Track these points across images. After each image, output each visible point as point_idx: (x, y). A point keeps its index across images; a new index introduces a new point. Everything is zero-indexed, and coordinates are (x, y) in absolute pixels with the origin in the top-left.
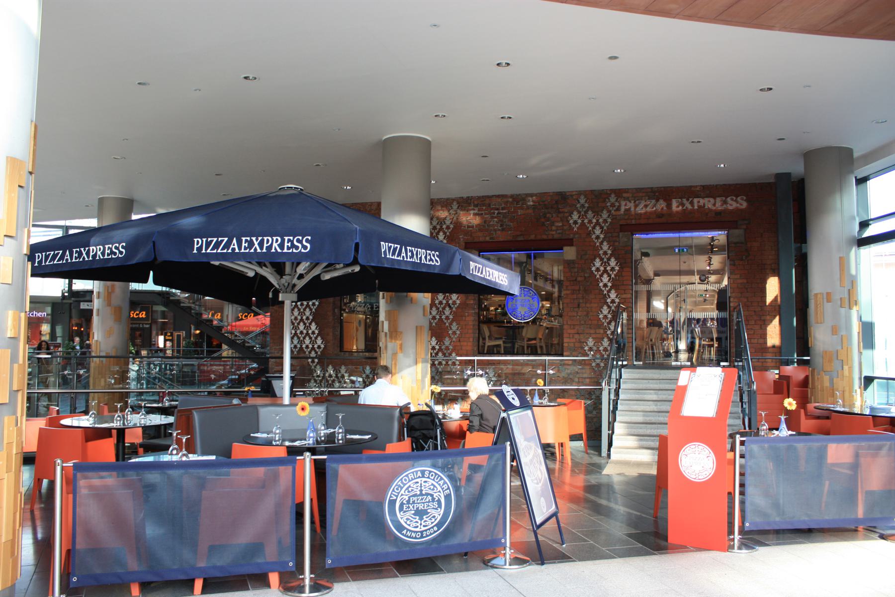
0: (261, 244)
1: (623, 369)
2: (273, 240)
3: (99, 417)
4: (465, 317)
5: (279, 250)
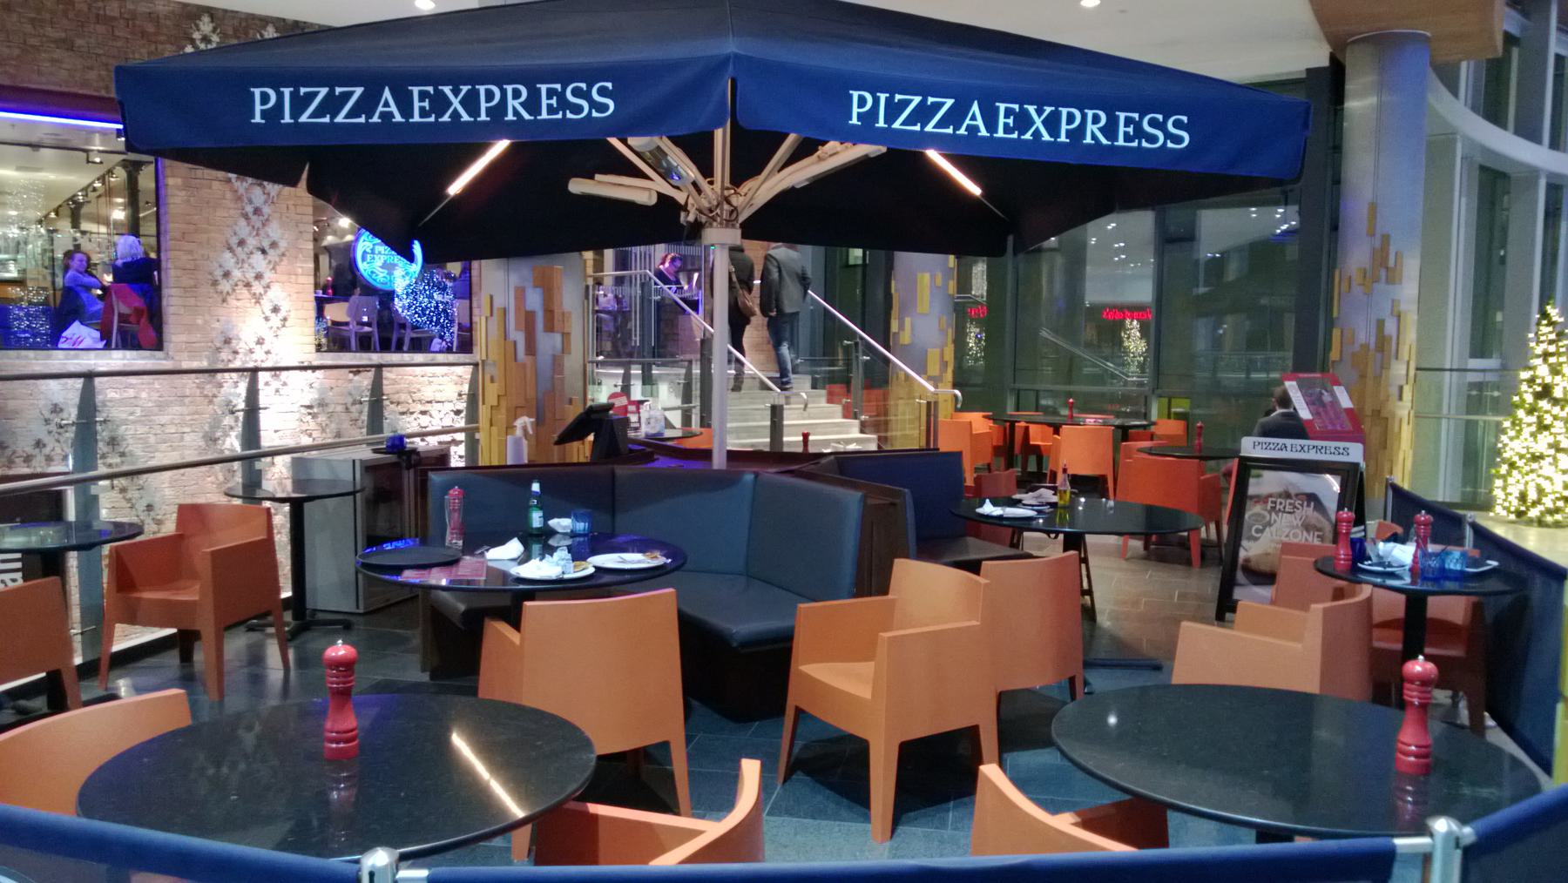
0: (1052, 124)
1: (469, 369)
2: (1084, 117)
3: (578, 555)
4: (296, 275)
5: (1104, 141)
